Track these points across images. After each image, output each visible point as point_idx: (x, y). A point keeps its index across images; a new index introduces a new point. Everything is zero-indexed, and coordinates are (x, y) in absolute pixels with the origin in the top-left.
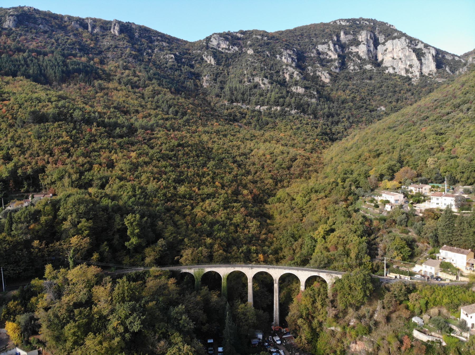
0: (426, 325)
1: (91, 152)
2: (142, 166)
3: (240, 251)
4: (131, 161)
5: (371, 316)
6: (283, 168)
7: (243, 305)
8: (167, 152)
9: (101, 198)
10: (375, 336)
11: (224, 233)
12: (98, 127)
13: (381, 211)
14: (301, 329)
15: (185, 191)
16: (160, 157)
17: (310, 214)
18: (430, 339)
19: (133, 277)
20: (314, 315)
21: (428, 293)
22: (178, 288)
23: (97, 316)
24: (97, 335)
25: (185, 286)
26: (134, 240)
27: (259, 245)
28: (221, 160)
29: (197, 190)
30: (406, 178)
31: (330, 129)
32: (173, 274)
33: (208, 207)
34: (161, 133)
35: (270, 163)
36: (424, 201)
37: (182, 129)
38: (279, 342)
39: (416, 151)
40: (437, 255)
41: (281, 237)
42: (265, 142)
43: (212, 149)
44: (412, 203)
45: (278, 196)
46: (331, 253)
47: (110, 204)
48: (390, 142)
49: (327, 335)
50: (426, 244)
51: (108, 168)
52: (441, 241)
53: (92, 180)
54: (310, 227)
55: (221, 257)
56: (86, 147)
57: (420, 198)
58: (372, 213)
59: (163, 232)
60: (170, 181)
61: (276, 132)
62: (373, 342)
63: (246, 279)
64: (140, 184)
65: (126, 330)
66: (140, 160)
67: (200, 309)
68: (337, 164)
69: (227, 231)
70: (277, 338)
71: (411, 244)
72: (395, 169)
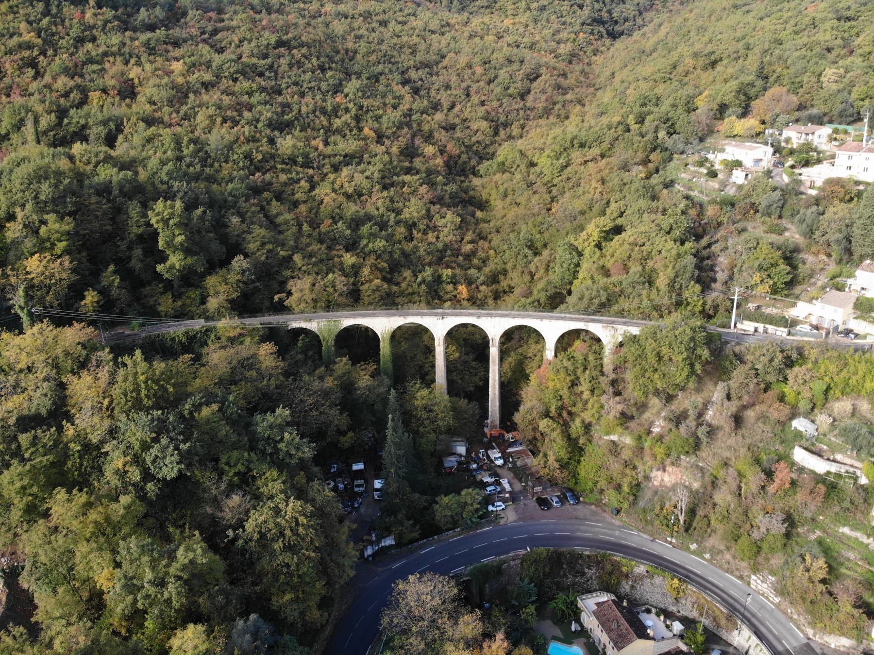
0: (821, 436)
1: (84, 63)
2: (196, 92)
3: (419, 279)
4: (172, 82)
5: (700, 415)
6: (510, 96)
7: (424, 392)
8: (254, 60)
9: (97, 164)
10: (708, 457)
11: (384, 242)
12: (100, 8)
13: (724, 185)
14: (547, 440)
15: (294, 146)
16: (237, 72)
17: (567, 195)
18: (834, 468)
19: (180, 342)
20: (574, 410)
21: (833, 368)
22: (282, 364)
23: (75, 447)
24: (75, 491)
25: (300, 356)
26: (175, 260)
27: (459, 265)
28: (376, 78)
29: (321, 146)
30: (777, 111)
31: (609, 12)
32: (271, 334)
33: (346, 185)
34: (240, 16)
35: (482, 83)
36: (819, 161)
37: (287, 9)
38: (500, 462)
39: (797, 54)
40: (850, 281)
41: (506, 247)
42: (471, 37)
43: (356, 52)
44: (793, 167)
45: (500, 159)
46: (615, 279)
47: (115, 179)
48: (739, 34)
49: (600, 452)
50: (823, 257)
51: (123, 98)
52: (857, 251)
53: (85, 127)
54: (568, 225)
55: (377, 294)
56: (72, 55)
57: (808, 157)
58: (707, 190)
59: (244, 239)
60: (260, 125)
61: (495, 17)
62: (701, 469)
63: (432, 338)
64: (192, 132)
65: (147, 476)
66: (192, 78)
67: (333, 405)
68: (626, 84)
69: (389, 238)
70: (495, 454)
71: (790, 256)
72: (752, 92)
